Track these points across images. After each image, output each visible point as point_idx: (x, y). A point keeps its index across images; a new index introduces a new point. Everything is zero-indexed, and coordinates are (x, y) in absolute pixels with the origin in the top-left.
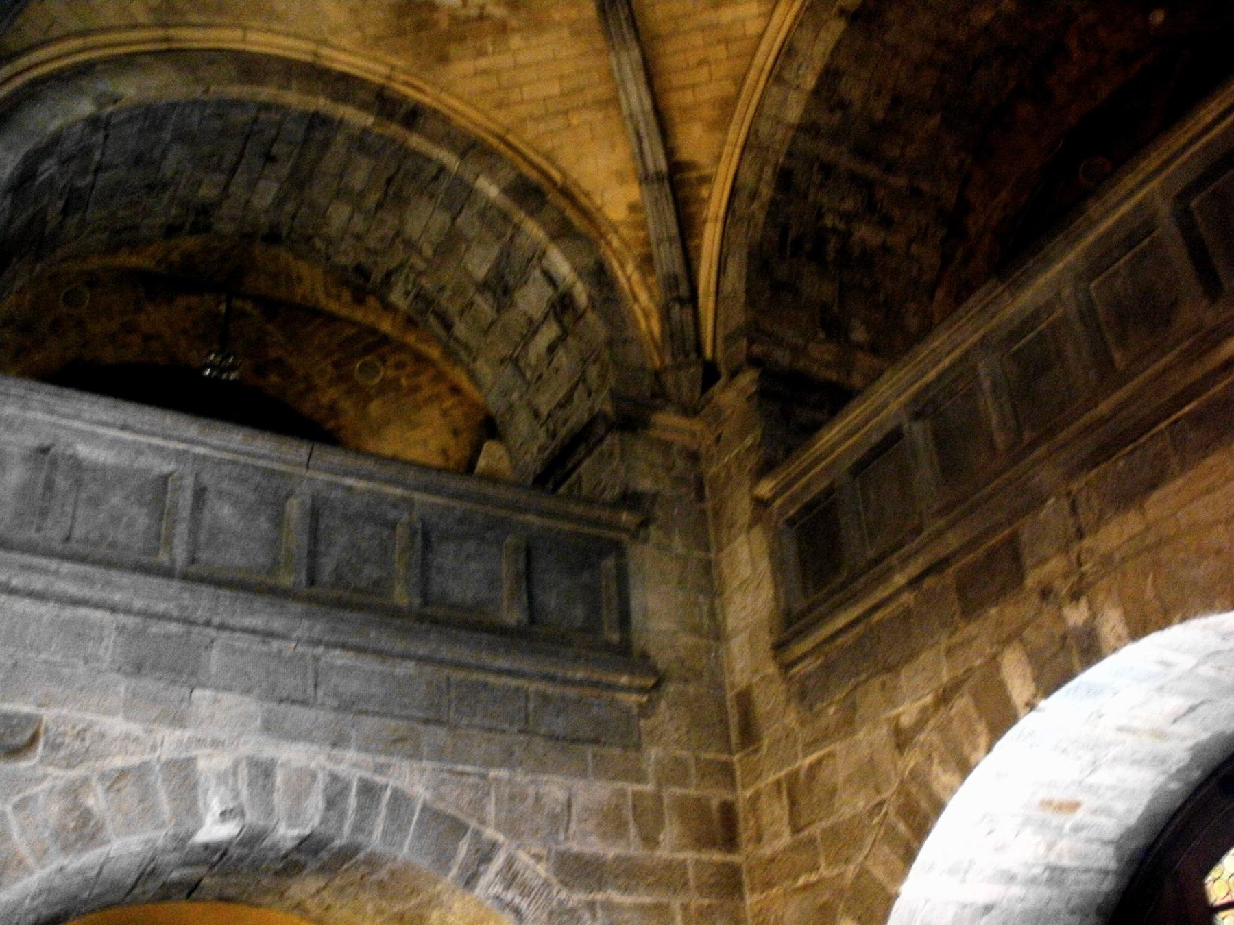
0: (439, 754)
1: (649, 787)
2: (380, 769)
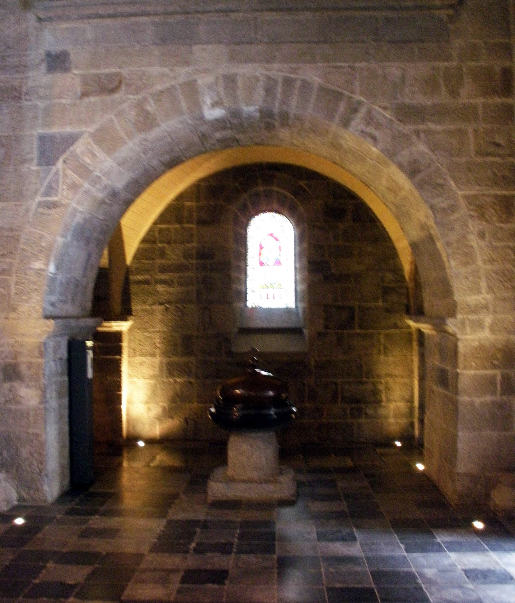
0: (326, 59)
1: (454, 64)
2: (294, 71)
